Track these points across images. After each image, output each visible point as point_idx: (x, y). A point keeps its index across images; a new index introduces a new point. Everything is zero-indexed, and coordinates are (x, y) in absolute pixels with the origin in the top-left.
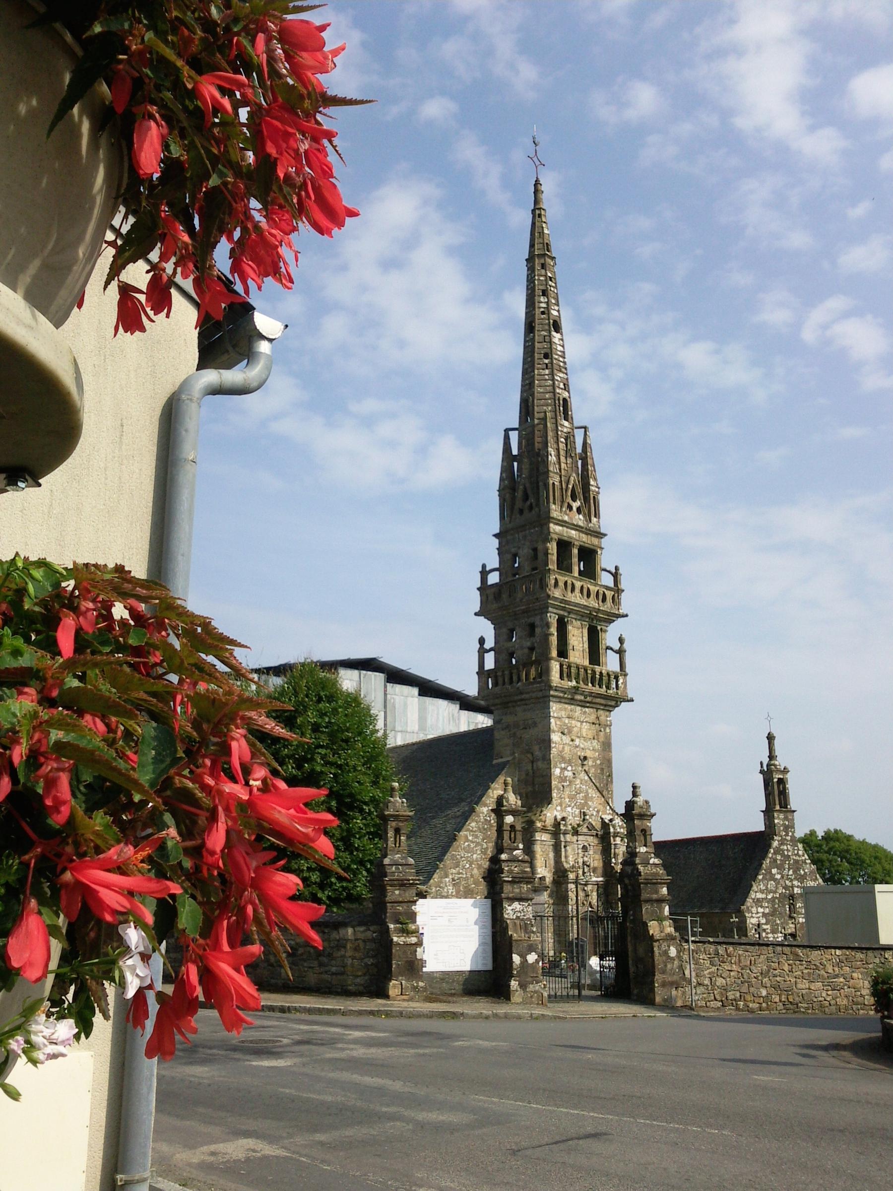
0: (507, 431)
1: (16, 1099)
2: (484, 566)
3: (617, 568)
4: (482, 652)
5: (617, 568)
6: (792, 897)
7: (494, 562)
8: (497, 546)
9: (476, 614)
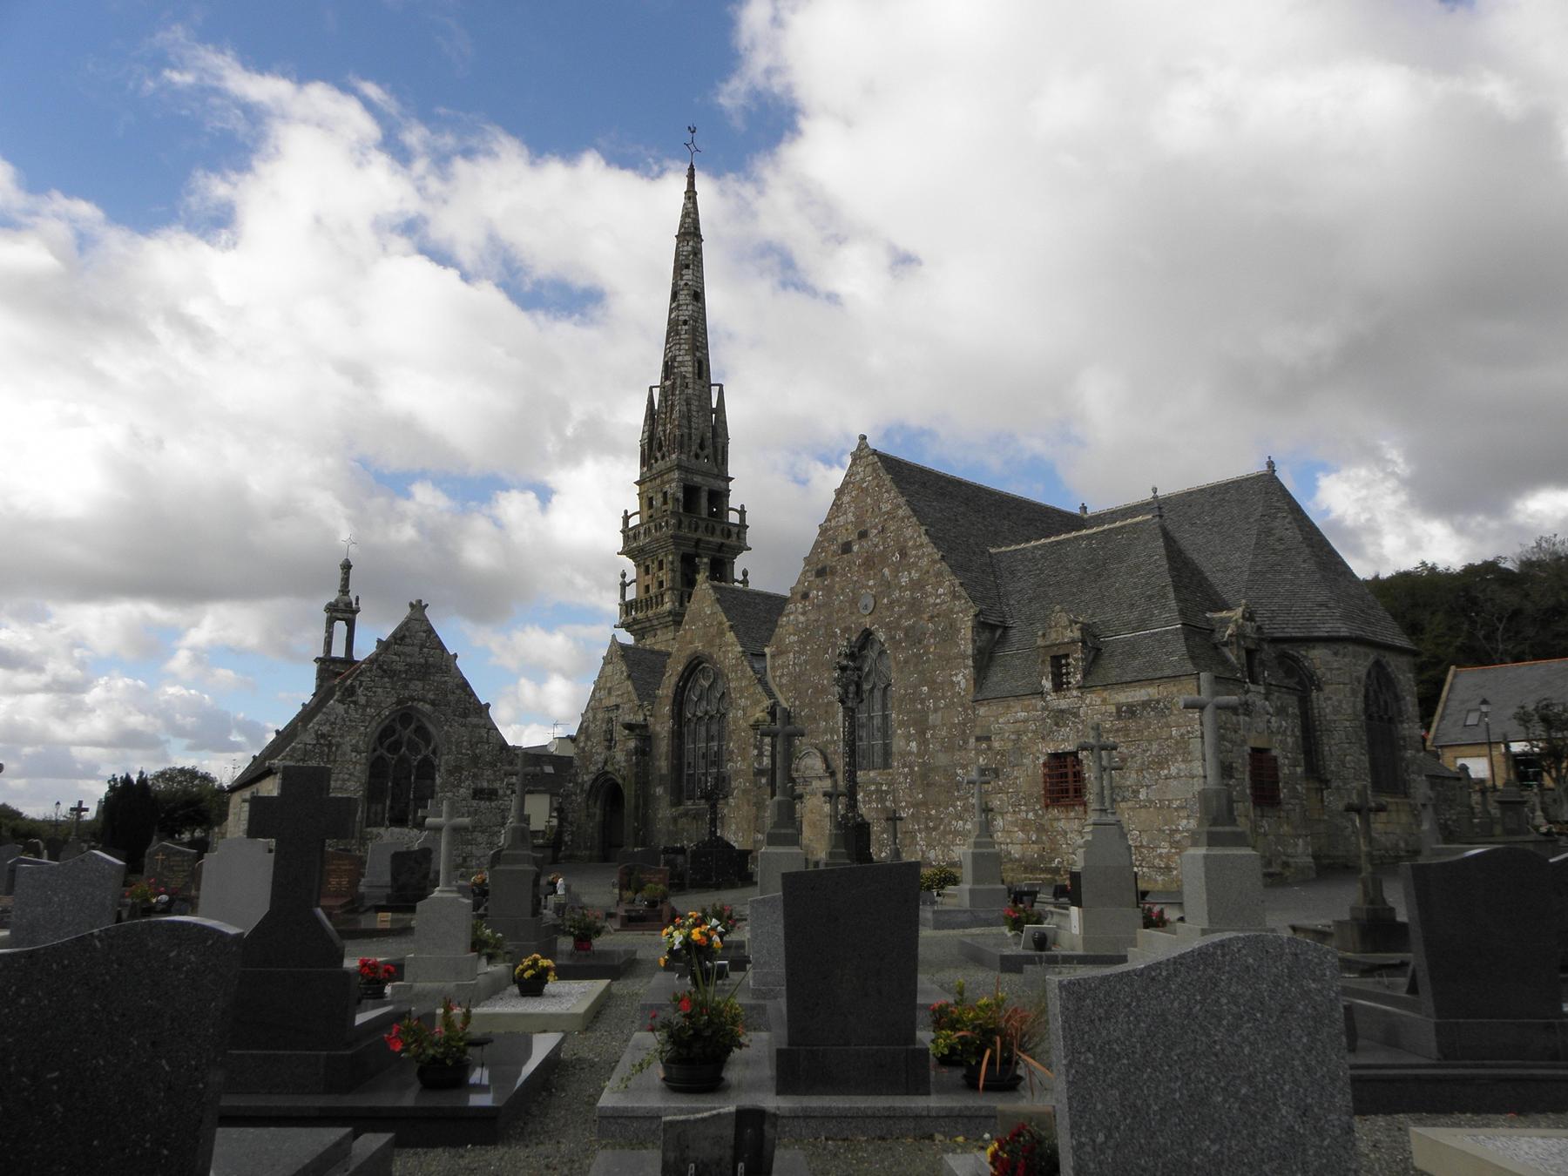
4: (624, 586)
7: (634, 505)
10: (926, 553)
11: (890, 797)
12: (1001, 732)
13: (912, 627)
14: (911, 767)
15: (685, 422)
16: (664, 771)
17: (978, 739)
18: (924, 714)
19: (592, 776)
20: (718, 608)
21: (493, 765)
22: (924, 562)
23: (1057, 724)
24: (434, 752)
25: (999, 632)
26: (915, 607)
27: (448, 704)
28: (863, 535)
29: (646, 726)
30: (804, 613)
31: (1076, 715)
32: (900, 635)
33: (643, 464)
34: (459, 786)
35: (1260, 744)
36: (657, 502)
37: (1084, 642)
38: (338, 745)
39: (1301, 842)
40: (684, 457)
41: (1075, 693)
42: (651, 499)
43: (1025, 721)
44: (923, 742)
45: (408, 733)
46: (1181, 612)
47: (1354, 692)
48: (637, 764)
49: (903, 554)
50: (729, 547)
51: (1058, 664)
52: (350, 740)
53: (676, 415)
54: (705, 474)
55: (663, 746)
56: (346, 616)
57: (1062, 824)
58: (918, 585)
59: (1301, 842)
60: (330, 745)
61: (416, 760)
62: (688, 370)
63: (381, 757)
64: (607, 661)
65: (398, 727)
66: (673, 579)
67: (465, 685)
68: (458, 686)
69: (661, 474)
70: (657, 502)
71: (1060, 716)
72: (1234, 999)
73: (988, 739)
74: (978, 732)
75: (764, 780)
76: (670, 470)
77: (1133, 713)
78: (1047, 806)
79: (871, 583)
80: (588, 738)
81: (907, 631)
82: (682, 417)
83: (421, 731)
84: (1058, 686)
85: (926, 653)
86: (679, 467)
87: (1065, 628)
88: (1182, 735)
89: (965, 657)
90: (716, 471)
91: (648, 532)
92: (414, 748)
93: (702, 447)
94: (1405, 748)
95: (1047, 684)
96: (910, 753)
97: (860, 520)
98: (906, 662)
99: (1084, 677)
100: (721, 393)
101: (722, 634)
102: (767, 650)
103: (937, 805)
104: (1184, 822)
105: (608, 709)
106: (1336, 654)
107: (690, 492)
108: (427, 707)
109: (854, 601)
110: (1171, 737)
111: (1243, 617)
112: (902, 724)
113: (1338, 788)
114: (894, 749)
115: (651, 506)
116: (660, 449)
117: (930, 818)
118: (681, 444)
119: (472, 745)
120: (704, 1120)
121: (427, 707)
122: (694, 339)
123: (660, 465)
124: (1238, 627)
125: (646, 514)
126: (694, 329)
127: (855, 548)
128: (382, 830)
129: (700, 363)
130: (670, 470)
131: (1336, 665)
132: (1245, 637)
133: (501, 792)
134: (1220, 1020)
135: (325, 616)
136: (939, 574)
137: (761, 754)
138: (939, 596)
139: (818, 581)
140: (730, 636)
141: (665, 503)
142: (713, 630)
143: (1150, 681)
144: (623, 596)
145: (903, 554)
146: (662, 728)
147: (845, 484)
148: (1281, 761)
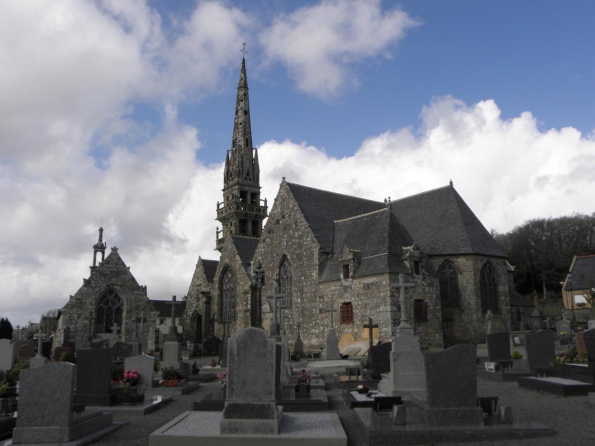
0: (228, 151)
1: (175, 296)
2: (218, 202)
3: (266, 199)
4: (218, 233)
5: (266, 199)
6: (222, 322)
7: (221, 200)
8: (193, 274)
9: (200, 257)
10: (304, 224)
11: (291, 320)
12: (327, 295)
13: (299, 253)
14: (298, 309)
15: (240, 165)
16: (216, 310)
17: (320, 297)
18: (302, 288)
19: (192, 312)
20: (233, 245)
21: (144, 309)
22: (303, 228)
23: (345, 292)
24: (122, 305)
25: (330, 255)
26: (300, 246)
27: (127, 286)
28: (283, 217)
29: (210, 293)
30: (264, 248)
31: (351, 288)
32: (295, 257)
33: (225, 183)
35: (419, 298)
36: (230, 198)
37: (354, 260)
38: (85, 303)
39: (437, 335)
40: (240, 179)
41: (350, 279)
42: (228, 197)
43: (335, 290)
44: (302, 299)
45: (112, 297)
46: (390, 248)
47: (475, 275)
48: (206, 307)
49: (296, 225)
50: (259, 216)
51: (346, 267)
52: (89, 301)
53: (237, 162)
54: (249, 186)
55: (216, 300)
56: (101, 250)
57: (346, 330)
58: (301, 237)
59: (437, 335)
60: (81, 303)
62: (242, 143)
63: (101, 307)
64: (197, 266)
65: (108, 295)
66: (236, 230)
67: (133, 279)
68: (130, 280)
69: (231, 187)
70: (230, 198)
71: (346, 288)
72: (52, 374)
73: (323, 297)
74: (320, 295)
75: (248, 314)
76: (234, 185)
77: (369, 287)
78: (341, 323)
80: (191, 297)
81: (297, 255)
82: (239, 163)
83: (117, 297)
84: (346, 276)
85: (303, 264)
86: (238, 184)
87: (348, 254)
88: (384, 296)
89: (315, 265)
90: (254, 185)
91: (226, 211)
92: (114, 303)
93: (248, 175)
94: (501, 295)
95: (342, 276)
96: (298, 303)
97: (282, 212)
98: (297, 267)
99: (353, 273)
100: (256, 152)
101: (235, 256)
102: (251, 262)
103: (307, 323)
104: (384, 329)
105: (197, 286)
106: (468, 260)
107: (243, 194)
108: (118, 288)
109: (280, 244)
110: (381, 296)
111: (413, 249)
112: (296, 292)
113: (468, 313)
114: (293, 302)
115: (228, 200)
116: (231, 176)
117: (304, 328)
118: (239, 174)
119: (136, 302)
121: (118, 288)
122: (245, 130)
123: (231, 183)
124: (411, 253)
125: (226, 204)
126: (245, 126)
127: (281, 222)
128: (102, 334)
129: (247, 140)
130: (234, 185)
131: (468, 264)
132: (413, 257)
134: (49, 377)
135: (93, 250)
136: (308, 233)
137: (247, 304)
138: (307, 242)
139: (268, 235)
140: (238, 258)
141: (233, 199)
142: (232, 255)
143: (374, 275)
144: (217, 237)
145: (296, 225)
146: (215, 293)
147: (278, 197)
148: (429, 304)
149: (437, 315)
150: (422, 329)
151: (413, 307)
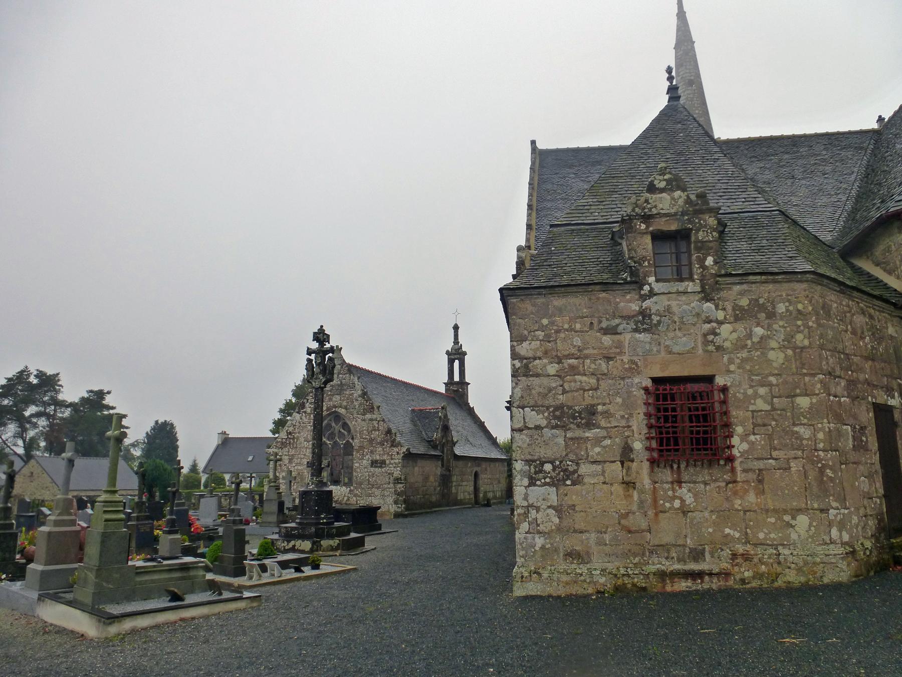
34: (363, 459)
38: (298, 438)
61: (342, 442)
79: (864, 439)
119: (370, 432)
120: (709, 592)
133: (387, 462)
149: (799, 438)
150: (696, 496)
151: (642, 410)
